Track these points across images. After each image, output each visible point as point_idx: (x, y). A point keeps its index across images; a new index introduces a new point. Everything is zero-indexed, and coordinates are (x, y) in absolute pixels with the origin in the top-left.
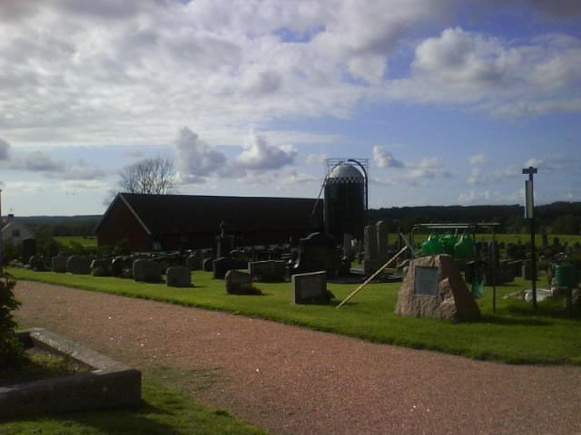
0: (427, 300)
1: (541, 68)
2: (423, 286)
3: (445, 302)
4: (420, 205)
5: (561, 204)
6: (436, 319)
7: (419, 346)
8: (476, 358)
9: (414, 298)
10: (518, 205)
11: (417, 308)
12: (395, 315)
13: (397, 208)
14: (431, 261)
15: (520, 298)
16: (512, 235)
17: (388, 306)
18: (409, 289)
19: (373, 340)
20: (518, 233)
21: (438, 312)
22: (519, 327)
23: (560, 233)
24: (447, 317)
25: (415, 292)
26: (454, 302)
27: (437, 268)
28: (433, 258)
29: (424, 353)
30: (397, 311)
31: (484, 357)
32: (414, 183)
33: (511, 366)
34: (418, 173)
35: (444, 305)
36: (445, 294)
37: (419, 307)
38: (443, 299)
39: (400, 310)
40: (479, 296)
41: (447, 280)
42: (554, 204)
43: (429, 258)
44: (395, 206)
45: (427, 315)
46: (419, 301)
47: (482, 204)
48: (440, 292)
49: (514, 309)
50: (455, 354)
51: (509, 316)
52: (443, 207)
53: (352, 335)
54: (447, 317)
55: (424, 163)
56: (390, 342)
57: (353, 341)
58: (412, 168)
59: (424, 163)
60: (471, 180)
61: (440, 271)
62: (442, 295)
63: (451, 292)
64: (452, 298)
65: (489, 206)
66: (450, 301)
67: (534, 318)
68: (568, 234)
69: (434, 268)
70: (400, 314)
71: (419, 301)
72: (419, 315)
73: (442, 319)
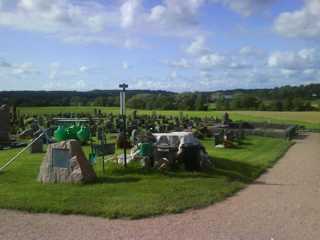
0: (62, 171)
1: (91, 19)
2: (59, 158)
3: (74, 172)
4: (20, 90)
5: (97, 90)
6: (69, 183)
7: (67, 213)
8: (112, 218)
9: (52, 170)
10: (76, 91)
11: (54, 177)
12: (38, 183)
13: (6, 92)
14: (64, 145)
15: (115, 161)
16: (74, 107)
17: (28, 173)
18: (48, 164)
19: (30, 210)
20: (76, 106)
21: (70, 179)
22: (122, 185)
23: (98, 106)
24: (76, 182)
25: (52, 166)
26: (80, 172)
27: (68, 150)
28: (66, 143)
29: (71, 217)
30: (39, 180)
31: (116, 216)
32: (18, 77)
33: (135, 221)
34: (20, 71)
35: (74, 174)
36: (74, 166)
37: (56, 175)
38: (73, 170)
39: (42, 178)
40: (93, 164)
41: (76, 157)
42: (93, 91)
43: (63, 142)
44: (5, 90)
45: (62, 181)
46: (56, 172)
47: (56, 90)
48: (70, 166)
49: (118, 171)
50: (95, 216)
51: (113, 177)
52: (35, 91)
53: (12, 208)
54: (76, 182)
55: (24, 65)
56: (44, 210)
57: (14, 214)
58: (18, 68)
59: (24, 65)
60: (52, 77)
61: (70, 152)
62: (72, 167)
63: (78, 165)
64: (80, 169)
65: (61, 91)
66: (78, 171)
67: (128, 176)
68: (101, 106)
69: (66, 150)
70: (42, 182)
71: (56, 172)
72: (56, 182)
73: (73, 183)
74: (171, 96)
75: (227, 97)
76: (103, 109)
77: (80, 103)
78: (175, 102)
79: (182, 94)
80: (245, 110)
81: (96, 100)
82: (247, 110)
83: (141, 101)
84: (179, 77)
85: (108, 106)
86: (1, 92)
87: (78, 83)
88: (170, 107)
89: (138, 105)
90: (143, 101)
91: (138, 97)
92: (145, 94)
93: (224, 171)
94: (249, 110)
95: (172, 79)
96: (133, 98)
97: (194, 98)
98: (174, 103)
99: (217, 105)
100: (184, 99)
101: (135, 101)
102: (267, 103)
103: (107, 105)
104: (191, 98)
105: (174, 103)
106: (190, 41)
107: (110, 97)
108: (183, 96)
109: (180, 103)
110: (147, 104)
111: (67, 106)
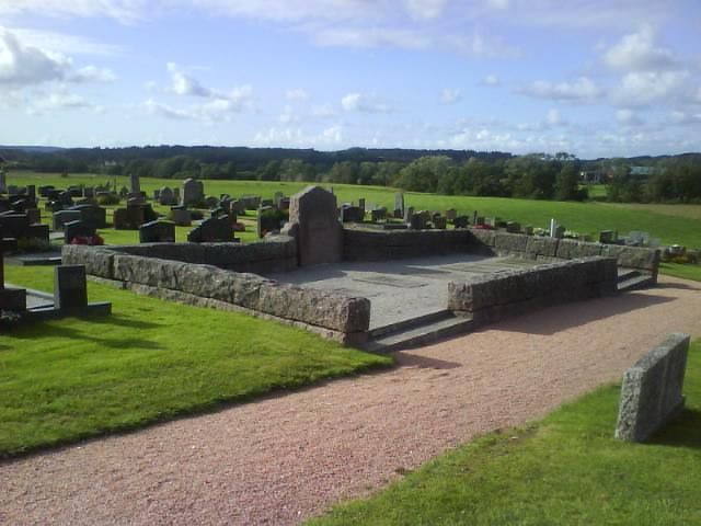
13: (167, 147)
23: (338, 182)
59: (236, 93)
60: (284, 118)
74: (498, 163)
75: (636, 170)
76: (340, 189)
77: (300, 177)
78: (506, 176)
79: (525, 158)
80: (682, 202)
81: (336, 168)
82: (687, 203)
83: (428, 173)
84: (564, 124)
85: (362, 183)
86: (698, 203)
87: (326, 133)
88: (495, 189)
89: (423, 182)
90: (432, 174)
91: (421, 164)
92: (439, 158)
93: (151, 244)
94: (693, 203)
95: (545, 127)
96: (412, 165)
97: (554, 169)
98: (503, 181)
99: (611, 189)
100: (528, 170)
101: (416, 174)
102: (599, 190)
103: (359, 181)
104: (545, 169)
105: (503, 181)
106: (615, 36)
107: (366, 163)
108: (525, 165)
109: (517, 181)
110: (440, 181)
111: (273, 180)
